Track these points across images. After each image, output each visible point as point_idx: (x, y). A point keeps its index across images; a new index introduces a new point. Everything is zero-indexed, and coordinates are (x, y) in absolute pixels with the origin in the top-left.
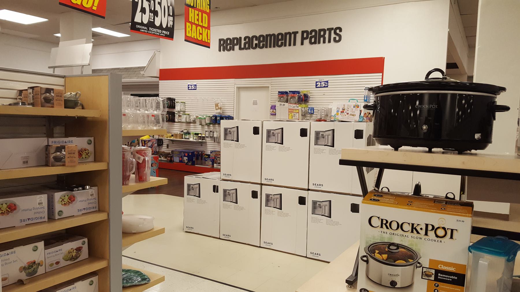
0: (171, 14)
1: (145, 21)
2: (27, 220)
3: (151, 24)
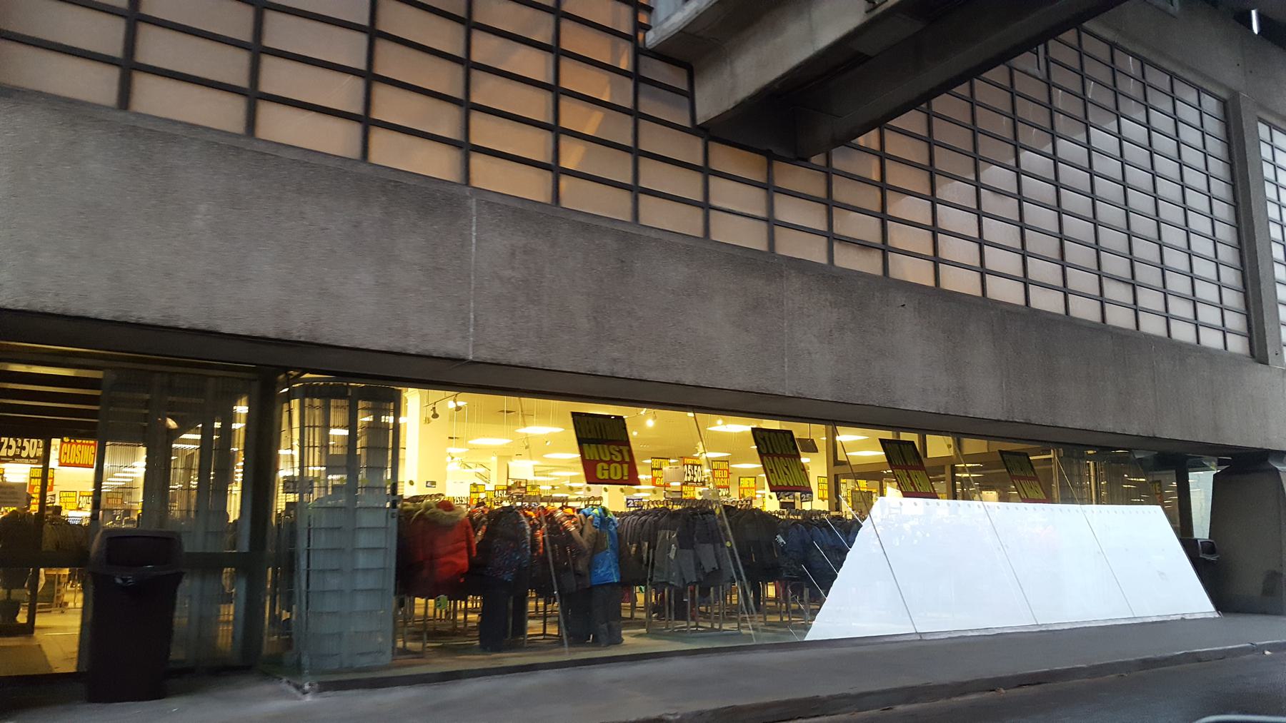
3: (692, 481)
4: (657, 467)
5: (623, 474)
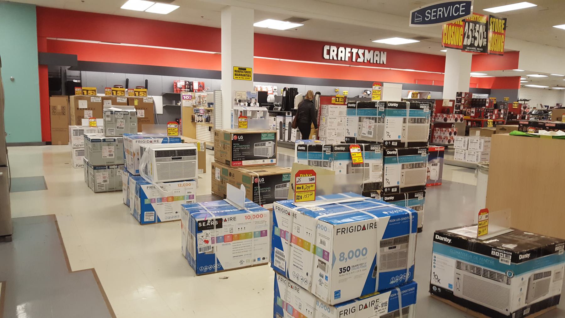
0: (485, 37)
1: (469, 44)
2: (227, 220)
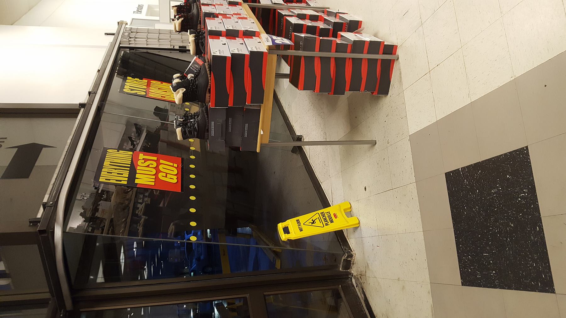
4: (126, 174)
5: (173, 166)
